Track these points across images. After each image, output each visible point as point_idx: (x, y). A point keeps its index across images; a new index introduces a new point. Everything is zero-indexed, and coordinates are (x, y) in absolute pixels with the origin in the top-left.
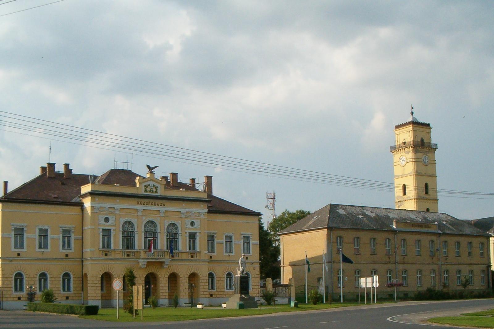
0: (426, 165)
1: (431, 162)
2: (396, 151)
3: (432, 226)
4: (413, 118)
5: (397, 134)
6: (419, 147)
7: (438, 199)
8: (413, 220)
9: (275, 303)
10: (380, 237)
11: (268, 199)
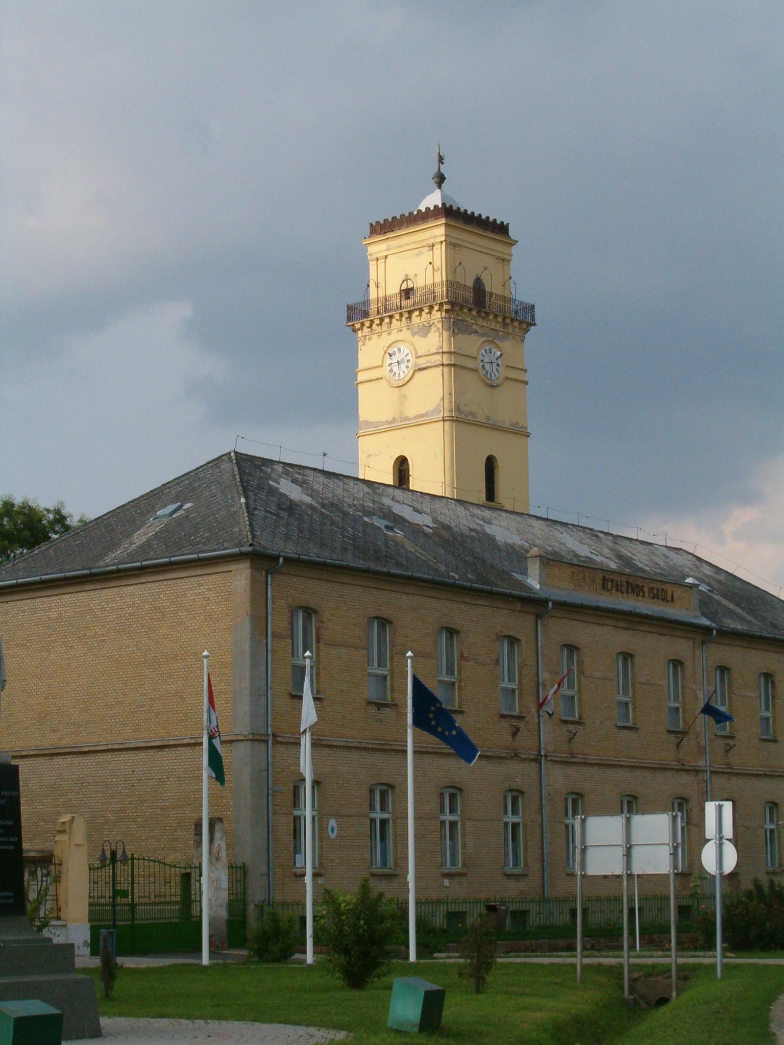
0: (492, 386)
2: (372, 322)
3: (678, 592)
5: (379, 255)
6: (470, 310)
10: (479, 622)
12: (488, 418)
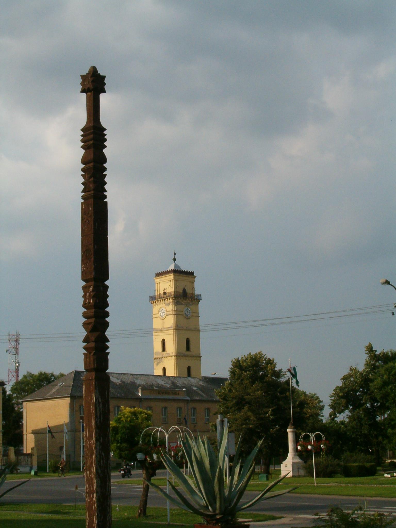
0: (188, 319)
1: (194, 314)
4: (176, 266)
8: (160, 387)
9: (17, 472)
11: (10, 341)
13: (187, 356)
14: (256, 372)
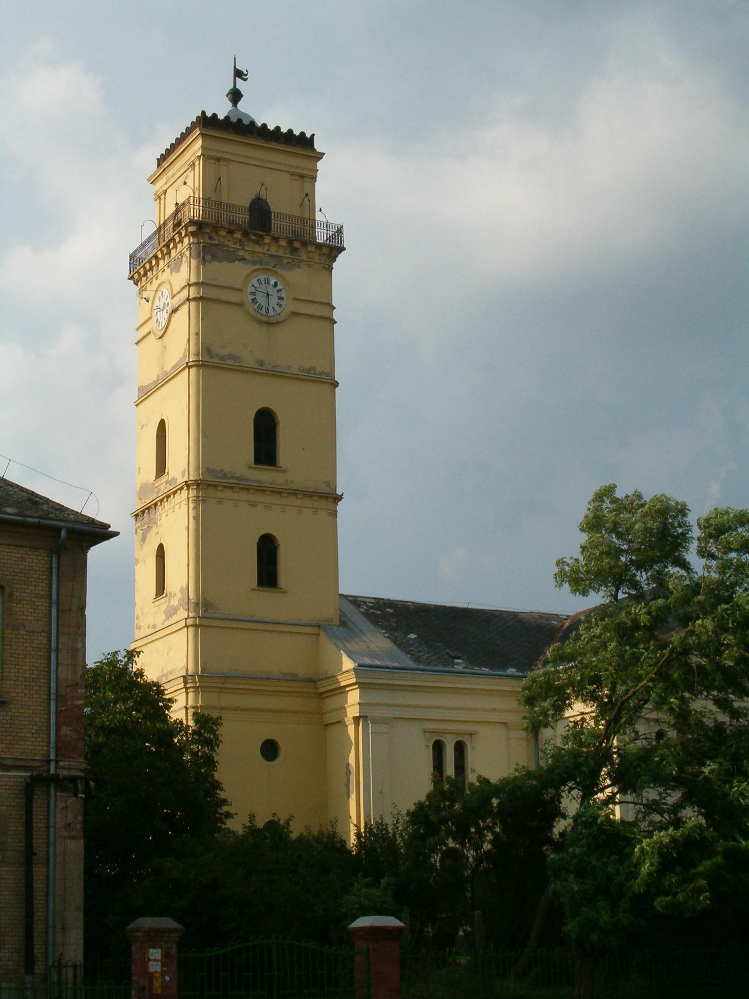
0: (268, 323)
7: (339, 492)
12: (261, 363)
13: (261, 489)
14: (714, 593)
